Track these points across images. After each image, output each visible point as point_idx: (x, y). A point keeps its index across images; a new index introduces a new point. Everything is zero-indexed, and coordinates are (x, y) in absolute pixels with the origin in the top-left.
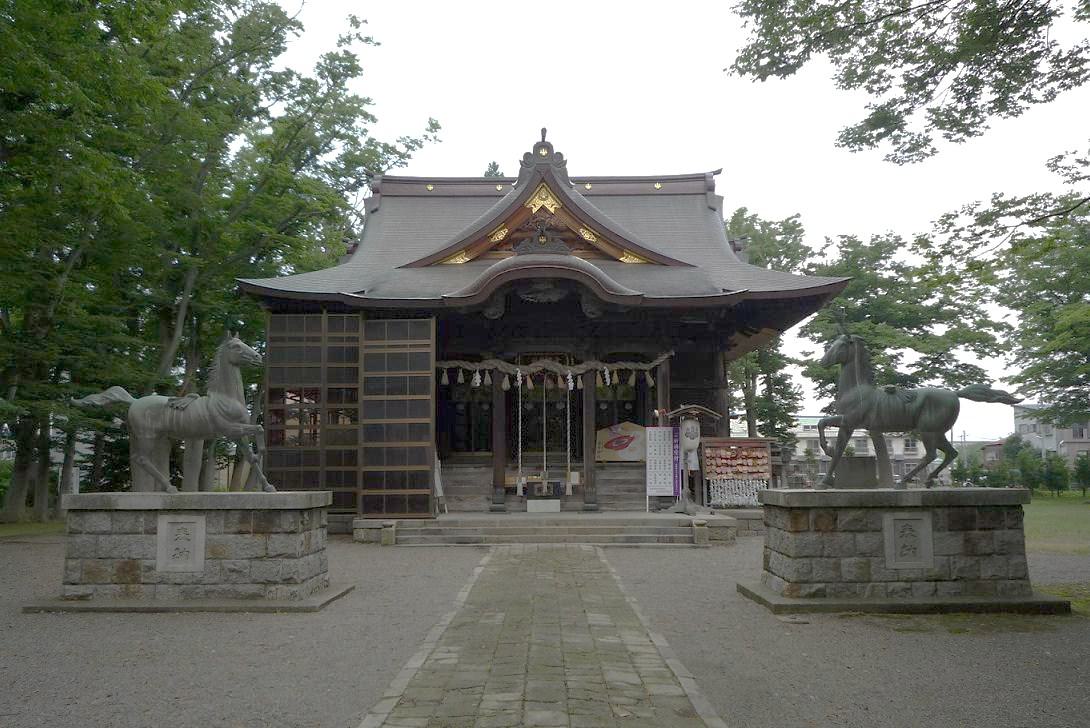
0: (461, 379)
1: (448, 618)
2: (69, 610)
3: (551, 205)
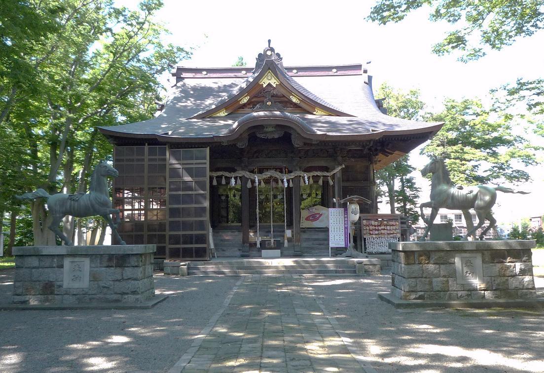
0: (224, 182)
1: (221, 311)
2: (18, 309)
3: (274, 82)
